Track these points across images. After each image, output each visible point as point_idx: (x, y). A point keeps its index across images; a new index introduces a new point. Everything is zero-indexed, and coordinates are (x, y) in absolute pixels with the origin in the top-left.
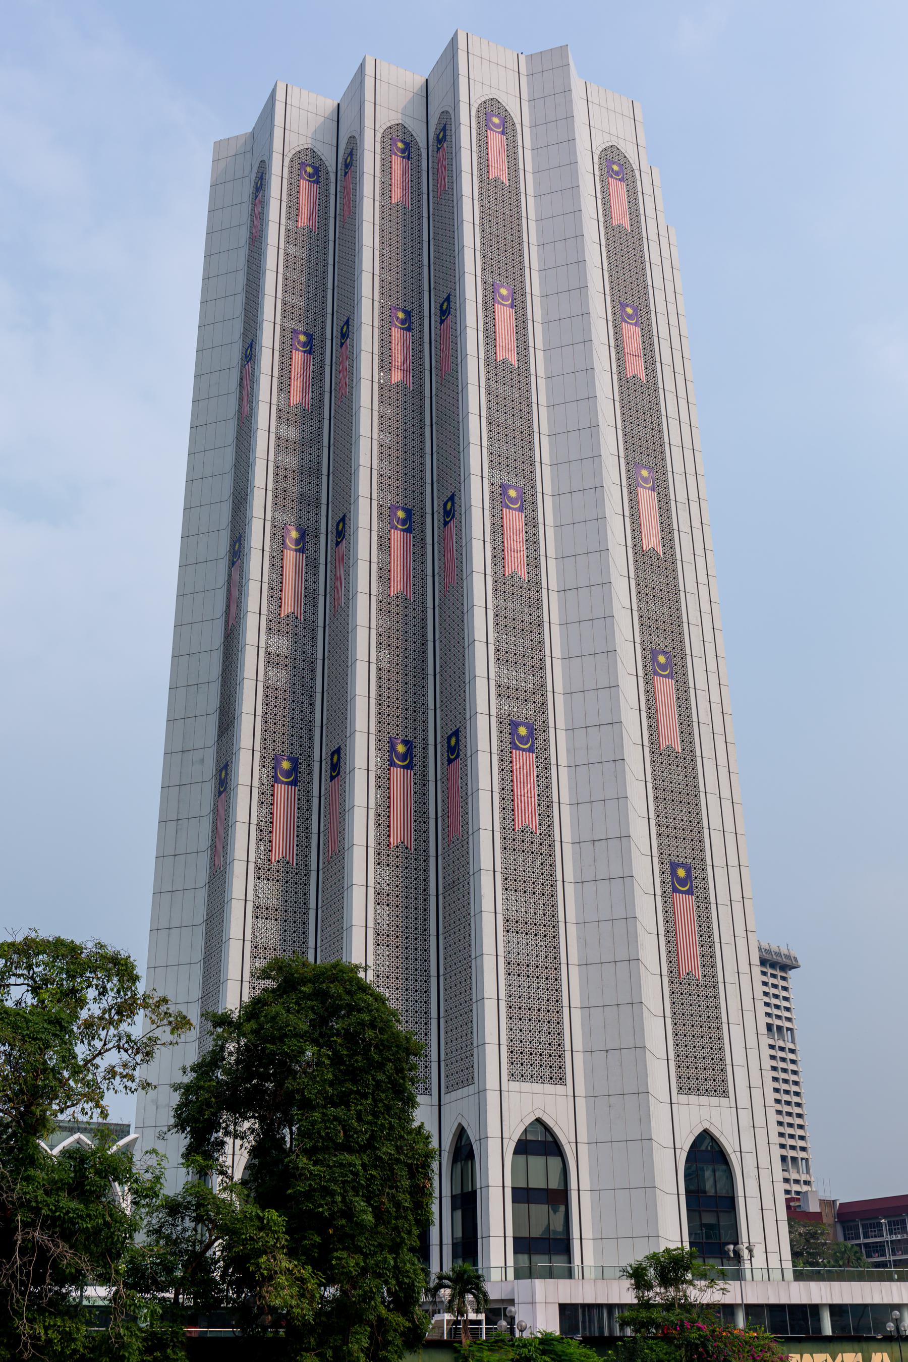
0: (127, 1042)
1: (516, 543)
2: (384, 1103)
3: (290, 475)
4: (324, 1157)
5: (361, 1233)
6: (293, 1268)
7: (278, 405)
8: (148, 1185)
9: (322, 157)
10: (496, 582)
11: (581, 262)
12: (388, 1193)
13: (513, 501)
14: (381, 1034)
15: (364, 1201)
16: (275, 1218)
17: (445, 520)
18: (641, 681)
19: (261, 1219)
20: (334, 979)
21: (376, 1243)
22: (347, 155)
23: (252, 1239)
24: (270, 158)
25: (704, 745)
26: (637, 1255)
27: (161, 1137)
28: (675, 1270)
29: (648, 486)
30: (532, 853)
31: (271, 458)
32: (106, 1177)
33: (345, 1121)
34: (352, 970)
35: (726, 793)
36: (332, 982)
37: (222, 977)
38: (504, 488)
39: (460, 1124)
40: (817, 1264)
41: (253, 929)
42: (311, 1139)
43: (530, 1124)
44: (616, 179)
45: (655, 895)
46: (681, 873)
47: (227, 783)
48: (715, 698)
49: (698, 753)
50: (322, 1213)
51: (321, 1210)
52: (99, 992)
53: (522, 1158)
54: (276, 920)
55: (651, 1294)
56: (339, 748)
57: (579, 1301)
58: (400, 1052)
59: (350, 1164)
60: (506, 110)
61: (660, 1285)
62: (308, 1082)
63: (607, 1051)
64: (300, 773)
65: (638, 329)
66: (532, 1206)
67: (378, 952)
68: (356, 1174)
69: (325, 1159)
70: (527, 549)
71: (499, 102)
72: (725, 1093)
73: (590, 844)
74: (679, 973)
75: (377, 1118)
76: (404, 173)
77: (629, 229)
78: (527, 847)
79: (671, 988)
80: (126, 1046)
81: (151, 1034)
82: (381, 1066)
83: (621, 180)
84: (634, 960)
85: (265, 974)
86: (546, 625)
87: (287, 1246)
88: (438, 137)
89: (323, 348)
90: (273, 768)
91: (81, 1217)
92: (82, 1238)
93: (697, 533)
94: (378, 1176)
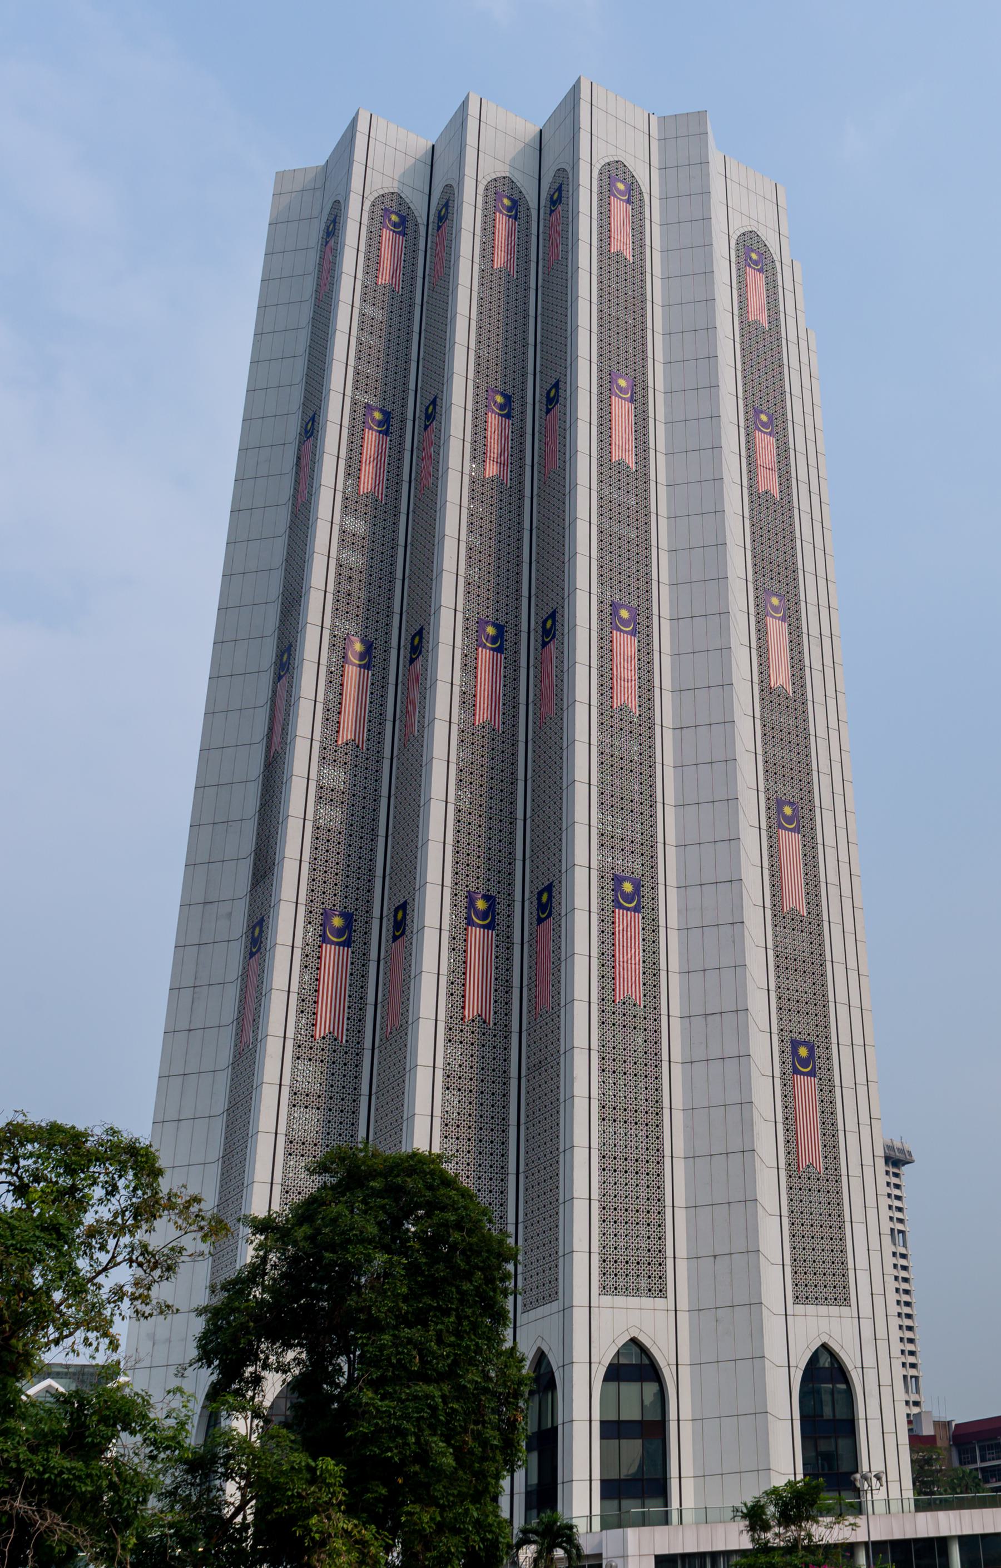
0: (142, 1254)
1: (626, 671)
2: (469, 1321)
3: (356, 576)
4: (394, 1390)
5: (439, 1481)
6: (352, 1529)
7: (344, 493)
8: (170, 1433)
9: (411, 205)
10: (602, 714)
11: (712, 358)
12: (473, 1430)
13: (625, 623)
14: (470, 1237)
15: (443, 1442)
16: (331, 1467)
17: (543, 640)
18: (764, 834)
19: (312, 1470)
20: (411, 1172)
21: (456, 1492)
22: (441, 206)
23: (299, 1495)
24: (347, 198)
25: (832, 909)
26: (749, 1494)
27: (181, 1373)
28: (798, 1507)
29: (778, 615)
30: (635, 1028)
31: (334, 553)
32: (114, 1425)
33: (421, 1343)
34: (433, 1161)
35: (852, 964)
36: (410, 1176)
37: (246, 1179)
38: (615, 607)
39: (539, 1349)
40: (933, 1493)
41: (289, 1120)
42: (378, 1367)
43: (624, 1345)
44: (755, 269)
45: (773, 1077)
46: (803, 1052)
47: (261, 942)
48: (843, 857)
49: (825, 917)
50: (392, 1458)
51: (389, 1454)
52: (107, 1191)
53: (613, 1386)
54: (318, 1109)
55: (769, 1535)
56: (405, 903)
57: (678, 1550)
58: (491, 1258)
59: (427, 1396)
60: (633, 176)
61: (779, 1525)
62: (376, 1298)
63: (715, 1256)
64: (355, 931)
65: (773, 440)
66: (623, 1442)
67: (445, 1146)
68: (434, 1409)
69: (395, 1392)
70: (639, 678)
71: (625, 166)
72: (846, 1302)
73: (701, 1019)
74: (799, 1166)
75: (461, 1338)
76: (510, 234)
77: (767, 327)
78: (629, 1021)
79: (789, 1183)
80: (141, 1259)
81: (174, 1244)
82: (468, 1276)
83: (760, 271)
84: (748, 1151)
85: (322, 1168)
86: (659, 767)
87: (345, 1501)
88: (552, 198)
89: (402, 429)
90: (321, 925)
91: (78, 1478)
92: (77, 1505)
93: (829, 672)
94: (460, 1409)
